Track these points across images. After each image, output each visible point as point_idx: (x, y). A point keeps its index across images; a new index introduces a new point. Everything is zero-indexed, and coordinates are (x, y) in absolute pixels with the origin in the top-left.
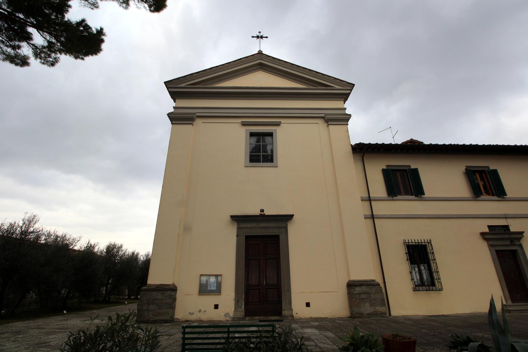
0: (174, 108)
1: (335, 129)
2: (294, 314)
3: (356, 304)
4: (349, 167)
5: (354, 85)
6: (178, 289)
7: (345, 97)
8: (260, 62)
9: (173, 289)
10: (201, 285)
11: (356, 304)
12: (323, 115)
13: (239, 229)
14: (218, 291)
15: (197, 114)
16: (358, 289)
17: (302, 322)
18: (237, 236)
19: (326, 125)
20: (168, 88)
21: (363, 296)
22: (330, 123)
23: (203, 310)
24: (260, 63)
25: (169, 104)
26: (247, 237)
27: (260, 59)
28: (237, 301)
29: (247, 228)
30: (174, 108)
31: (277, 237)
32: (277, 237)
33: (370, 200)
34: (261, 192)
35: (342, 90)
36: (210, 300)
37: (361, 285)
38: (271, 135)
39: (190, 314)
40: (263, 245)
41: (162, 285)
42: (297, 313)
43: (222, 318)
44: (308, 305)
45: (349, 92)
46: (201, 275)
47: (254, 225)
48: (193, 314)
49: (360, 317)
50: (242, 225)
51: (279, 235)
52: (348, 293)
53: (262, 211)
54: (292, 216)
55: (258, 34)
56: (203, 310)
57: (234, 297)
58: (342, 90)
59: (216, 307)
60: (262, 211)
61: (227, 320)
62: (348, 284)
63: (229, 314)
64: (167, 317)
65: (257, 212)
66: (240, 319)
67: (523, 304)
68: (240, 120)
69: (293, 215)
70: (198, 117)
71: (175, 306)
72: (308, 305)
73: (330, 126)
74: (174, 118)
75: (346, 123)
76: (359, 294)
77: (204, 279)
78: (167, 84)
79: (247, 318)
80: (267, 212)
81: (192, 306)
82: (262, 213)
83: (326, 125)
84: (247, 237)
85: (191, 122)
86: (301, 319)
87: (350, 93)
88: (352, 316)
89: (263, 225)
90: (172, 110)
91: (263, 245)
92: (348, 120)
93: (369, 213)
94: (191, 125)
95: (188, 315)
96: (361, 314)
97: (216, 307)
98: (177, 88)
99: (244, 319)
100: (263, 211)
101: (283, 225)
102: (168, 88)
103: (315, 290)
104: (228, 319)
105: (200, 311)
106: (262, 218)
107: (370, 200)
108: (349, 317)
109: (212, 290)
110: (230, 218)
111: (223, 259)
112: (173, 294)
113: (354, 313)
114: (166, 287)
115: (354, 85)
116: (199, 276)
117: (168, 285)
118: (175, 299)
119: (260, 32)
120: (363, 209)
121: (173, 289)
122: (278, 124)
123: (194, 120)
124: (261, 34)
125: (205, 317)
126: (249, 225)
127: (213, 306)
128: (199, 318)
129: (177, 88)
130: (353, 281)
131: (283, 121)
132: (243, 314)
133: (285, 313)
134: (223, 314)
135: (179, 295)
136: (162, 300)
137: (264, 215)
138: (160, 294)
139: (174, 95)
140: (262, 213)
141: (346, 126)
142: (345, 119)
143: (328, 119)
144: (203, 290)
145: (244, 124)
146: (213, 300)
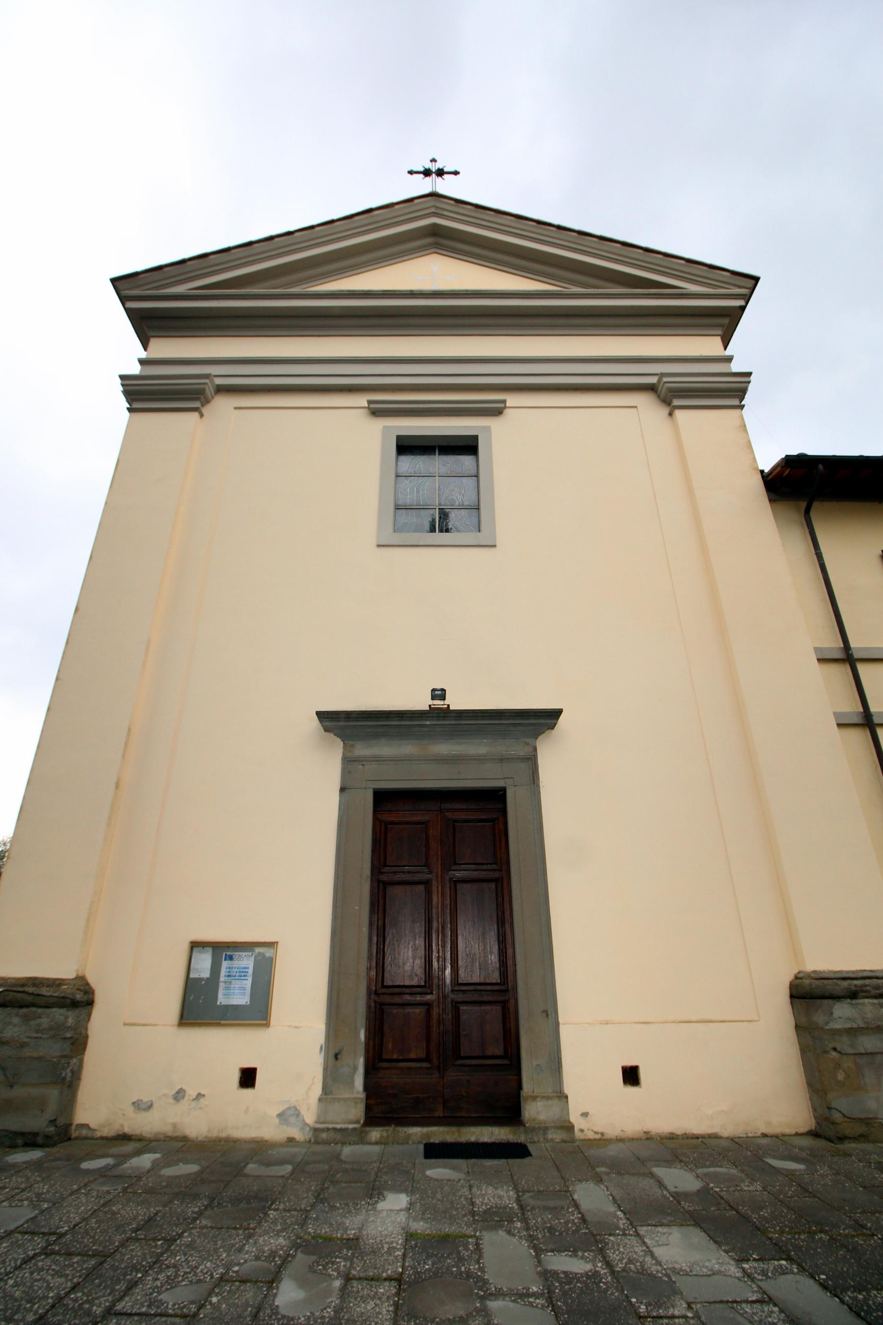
0: (142, 362)
1: (698, 424)
2: (574, 1118)
3: (841, 1076)
4: (767, 542)
5: (756, 279)
6: (99, 999)
7: (726, 322)
8: (438, 224)
9: (78, 999)
10: (191, 986)
11: (841, 1076)
12: (654, 380)
13: (348, 762)
14: (258, 1012)
15: (219, 381)
16: (843, 1013)
17: (618, 1167)
18: (342, 790)
19: (665, 411)
20: (123, 299)
21: (868, 1043)
22: (676, 402)
23: (192, 1093)
24: (435, 225)
25: (126, 352)
26: (382, 798)
27: (435, 214)
28: (334, 1055)
29: (378, 759)
30: (142, 362)
31: (495, 798)
32: (495, 798)
33: (848, 658)
34: (438, 637)
35: (718, 300)
36: (225, 1048)
37: (853, 995)
38: (467, 446)
39: (138, 1106)
40: (442, 827)
41: (35, 982)
42: (585, 1115)
43: (272, 1131)
44: (631, 1076)
45: (741, 303)
46: (195, 945)
47: (408, 748)
48: (150, 1106)
49: (862, 1137)
50: (362, 750)
51: (503, 790)
52: (798, 1027)
53: (439, 694)
54: (554, 715)
55: (428, 165)
56: (192, 1093)
57: (321, 1039)
58: (718, 300)
59: (248, 1078)
60: (439, 694)
61: (291, 1140)
62: (792, 986)
63: (298, 1114)
64: (36, 1123)
65: (422, 702)
66: (344, 1136)
67: (464, 806)
68: (362, 400)
69: (554, 715)
70: (223, 390)
71: (77, 1075)
72: (631, 1076)
73: (678, 413)
74: (140, 394)
75: (736, 402)
76: (852, 1032)
77: (203, 964)
78: (116, 283)
79: (375, 1134)
80: (456, 701)
81: (147, 1075)
82: (438, 703)
83: (664, 411)
84: (382, 798)
85: (197, 404)
86: (603, 1141)
87: (743, 309)
88: (827, 1131)
89: (444, 748)
90: (135, 369)
91: (442, 827)
92: (741, 393)
93: (851, 707)
94: (196, 415)
95: (130, 1110)
96: (867, 1121)
97: (248, 1078)
98: (154, 301)
99: (359, 1136)
100: (443, 697)
101: (517, 749)
102: (123, 300)
103: (654, 1013)
104: (297, 1134)
105: (179, 1095)
106: (440, 720)
107: (848, 658)
108: (814, 1134)
109: (236, 1007)
110: (777, 1016)
111: (282, 876)
112: (70, 1021)
113: (837, 1116)
114: (45, 991)
115: (756, 279)
116: (186, 947)
117: (56, 983)
118: (78, 1043)
119: (433, 160)
120: (830, 692)
121: (78, 999)
122: (497, 411)
123: (208, 401)
124: (439, 165)
125: (197, 1124)
126: (386, 749)
127: (236, 1076)
128: (174, 1125)
129: (154, 301)
130: (821, 977)
131: (512, 400)
132: (358, 1112)
133: (534, 1111)
134: (274, 1111)
135: (99, 1023)
136: (23, 1045)
137: (446, 713)
138: (16, 1020)
139: (146, 324)
140: (438, 703)
141: (735, 413)
142: (732, 391)
143: (671, 390)
144: (199, 1006)
145: (376, 412)
146: (232, 1047)
